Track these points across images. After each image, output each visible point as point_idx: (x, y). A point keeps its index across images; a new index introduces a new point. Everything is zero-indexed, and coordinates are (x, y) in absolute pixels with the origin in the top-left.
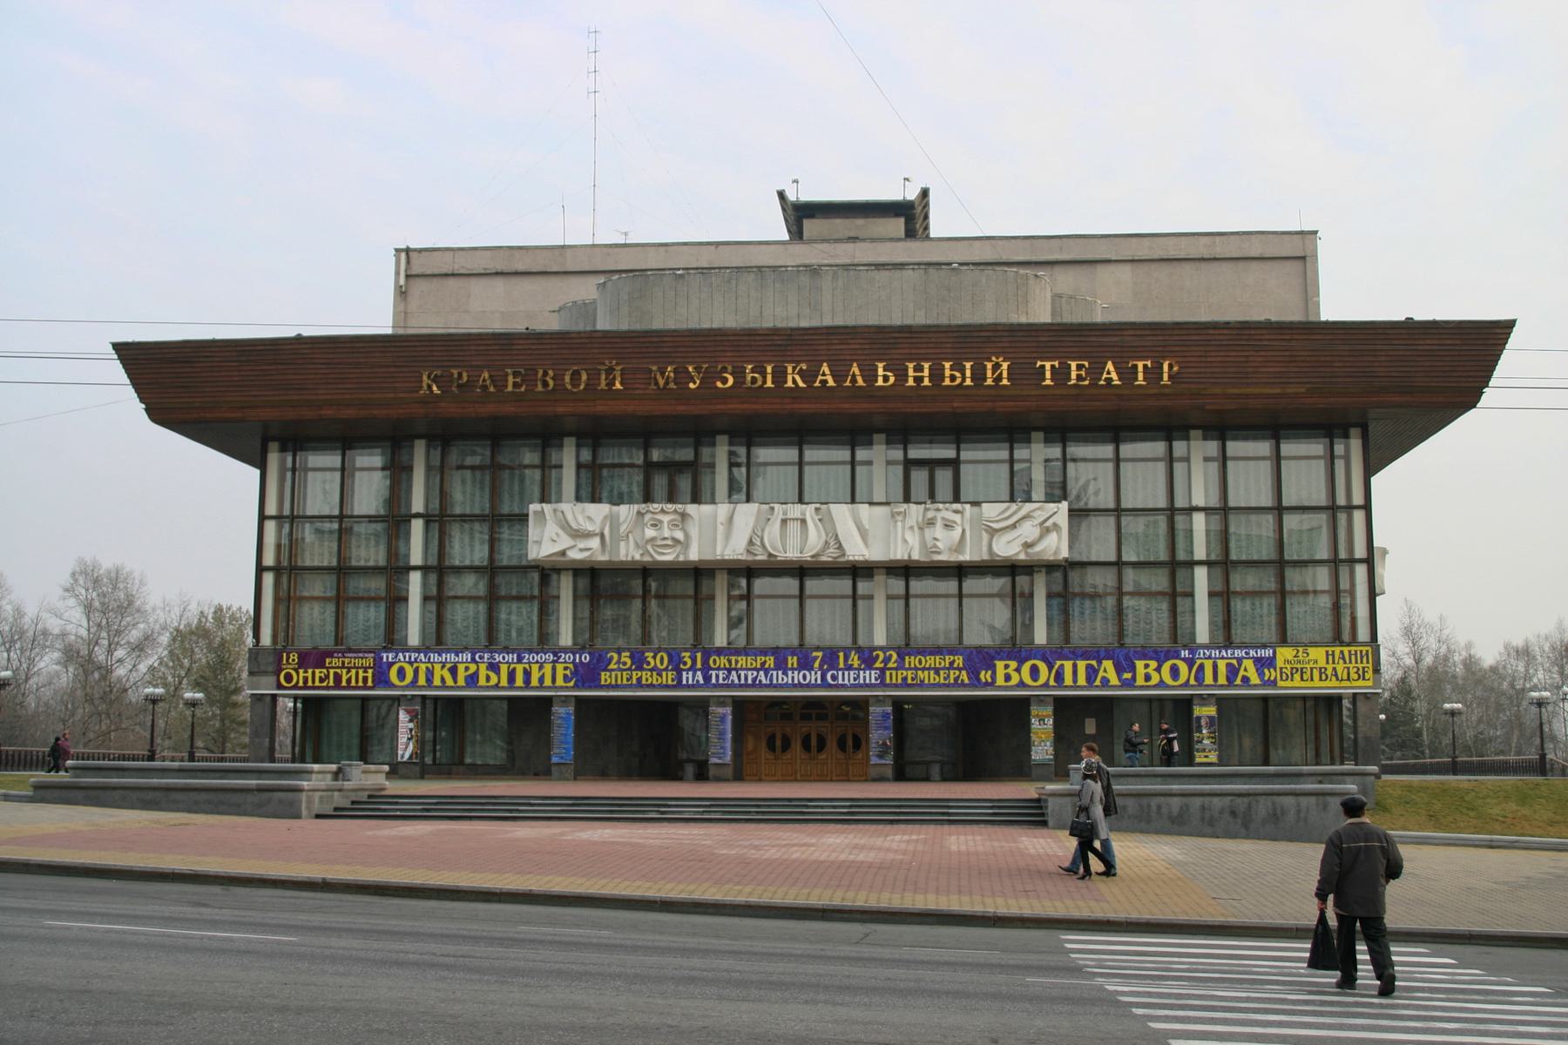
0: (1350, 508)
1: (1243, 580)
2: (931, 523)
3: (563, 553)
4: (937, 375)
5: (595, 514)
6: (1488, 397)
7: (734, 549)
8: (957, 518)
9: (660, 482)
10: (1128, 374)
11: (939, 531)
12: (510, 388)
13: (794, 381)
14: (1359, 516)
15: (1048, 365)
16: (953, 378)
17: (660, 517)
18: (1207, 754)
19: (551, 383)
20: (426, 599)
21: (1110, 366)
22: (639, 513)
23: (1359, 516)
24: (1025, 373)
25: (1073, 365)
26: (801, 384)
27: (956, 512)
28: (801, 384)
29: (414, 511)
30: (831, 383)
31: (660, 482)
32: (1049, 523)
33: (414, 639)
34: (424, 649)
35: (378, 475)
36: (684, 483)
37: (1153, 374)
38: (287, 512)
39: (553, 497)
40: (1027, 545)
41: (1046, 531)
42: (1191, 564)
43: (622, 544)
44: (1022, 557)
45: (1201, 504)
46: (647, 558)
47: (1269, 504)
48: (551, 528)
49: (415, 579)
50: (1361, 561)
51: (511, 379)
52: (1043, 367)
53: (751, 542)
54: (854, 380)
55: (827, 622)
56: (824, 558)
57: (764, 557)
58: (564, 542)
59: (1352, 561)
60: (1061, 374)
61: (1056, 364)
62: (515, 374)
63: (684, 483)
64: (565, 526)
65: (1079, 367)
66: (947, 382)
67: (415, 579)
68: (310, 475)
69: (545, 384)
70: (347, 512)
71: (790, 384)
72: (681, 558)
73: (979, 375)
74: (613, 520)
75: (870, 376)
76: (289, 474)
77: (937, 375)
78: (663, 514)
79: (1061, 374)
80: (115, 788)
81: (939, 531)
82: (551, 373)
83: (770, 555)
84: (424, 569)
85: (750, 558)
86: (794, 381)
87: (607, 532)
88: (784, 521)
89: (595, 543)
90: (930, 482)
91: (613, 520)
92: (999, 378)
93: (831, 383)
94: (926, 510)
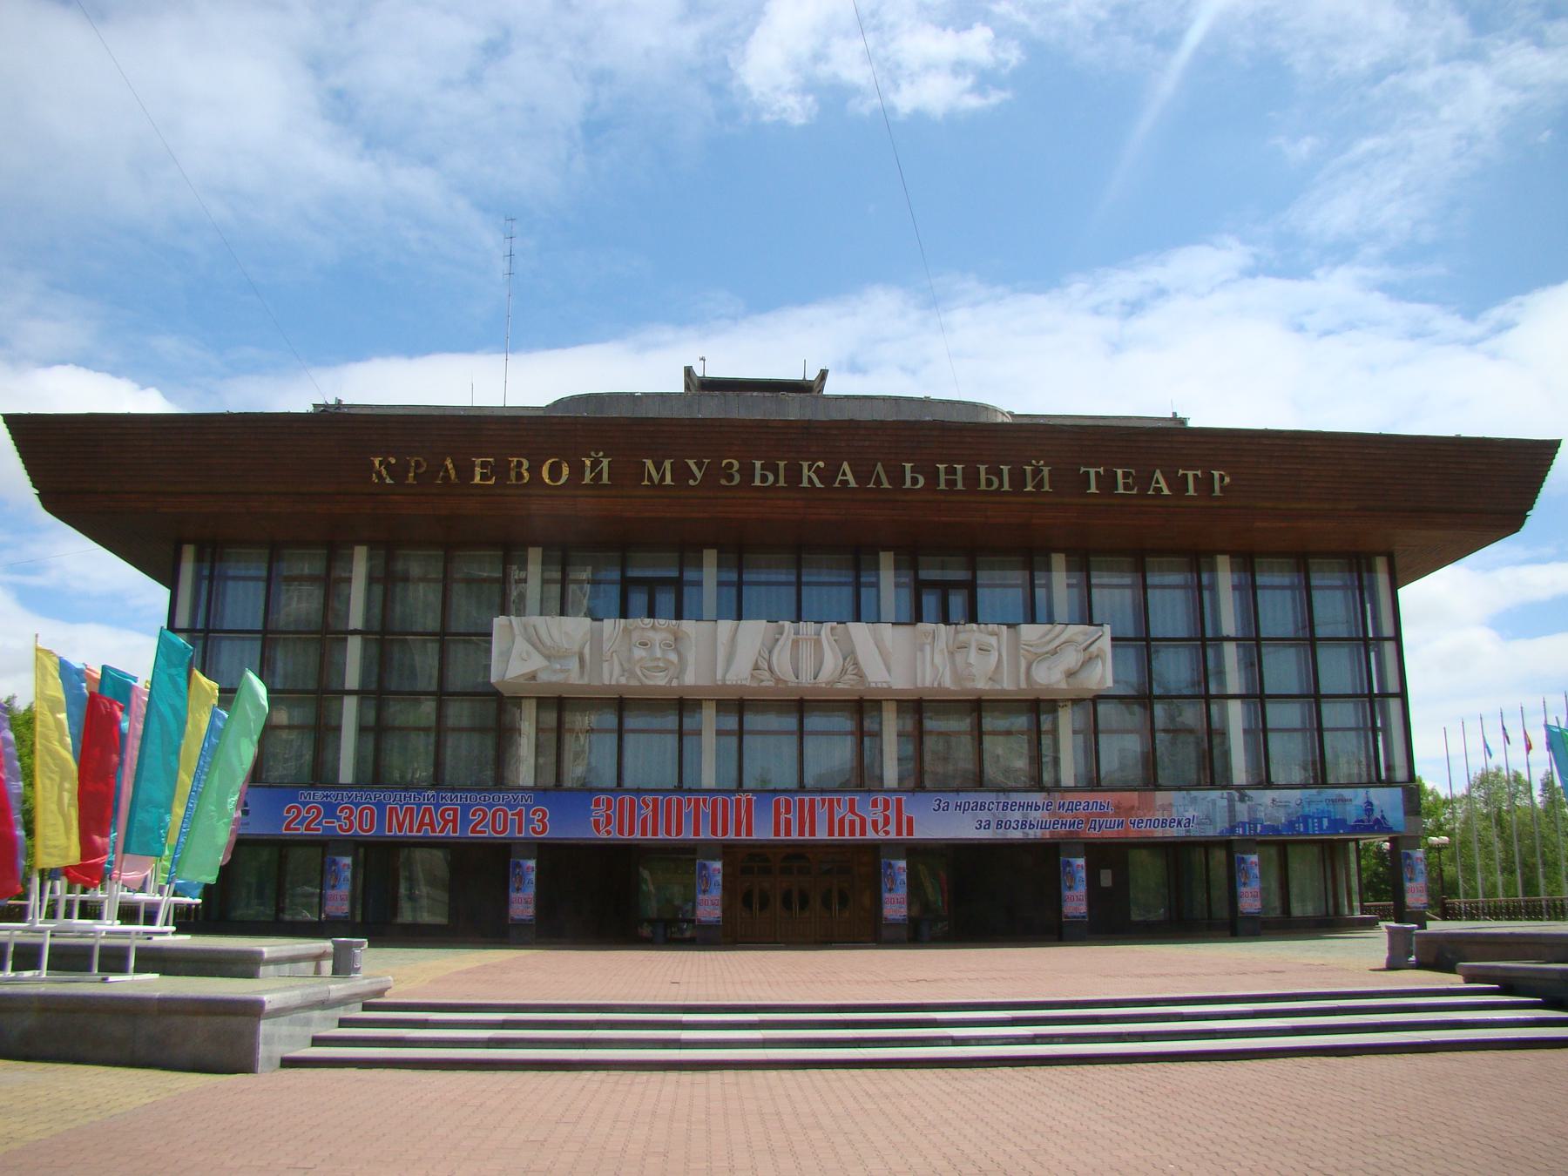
0: (1379, 639)
1: (400, 714)
2: (964, 647)
3: (533, 677)
4: (972, 477)
5: (574, 629)
6: (1534, 517)
7: (739, 674)
8: (993, 640)
9: (930, 601)
10: (1179, 485)
11: (973, 656)
12: (477, 480)
13: (810, 480)
14: (1389, 647)
15: (1092, 471)
16: (764, 478)
17: (651, 634)
18: (100, 894)
19: (526, 474)
20: (362, 729)
21: (1158, 474)
22: (625, 629)
23: (1389, 647)
24: (627, 473)
25: (1119, 472)
26: (819, 485)
27: (993, 634)
28: (819, 485)
29: (352, 626)
30: (853, 484)
31: (930, 601)
32: (1093, 648)
33: (346, 774)
34: (359, 784)
35: (1179, 595)
36: (957, 601)
37: (1205, 484)
38: (200, 626)
39: (513, 608)
40: (1070, 674)
41: (1089, 661)
42: (360, 693)
43: (606, 666)
44: (1063, 685)
45: (1232, 633)
46: (634, 682)
47: (1182, 632)
48: (521, 645)
49: (350, 706)
50: (1393, 695)
51: (478, 470)
52: (1087, 473)
53: (756, 667)
54: (878, 481)
55: (771, 758)
56: (840, 686)
57: (772, 684)
58: (536, 662)
59: (1384, 695)
60: (1108, 482)
61: (1101, 470)
62: (484, 465)
63: (957, 601)
64: (536, 643)
65: (1126, 475)
66: (757, 483)
67: (350, 706)
68: (230, 584)
69: (520, 476)
70: (272, 626)
71: (805, 484)
72: (675, 683)
73: (1018, 479)
74: (596, 639)
75: (897, 477)
76: (205, 584)
77: (972, 477)
78: (655, 631)
79: (1108, 482)
80: (1496, 913)
81: (973, 656)
82: (526, 464)
83: (778, 680)
84: (360, 693)
85: (755, 684)
86: (810, 480)
87: (587, 651)
88: (796, 643)
89: (574, 664)
90: (942, 598)
91: (596, 639)
92: (1039, 485)
93: (853, 484)
94: (957, 632)
